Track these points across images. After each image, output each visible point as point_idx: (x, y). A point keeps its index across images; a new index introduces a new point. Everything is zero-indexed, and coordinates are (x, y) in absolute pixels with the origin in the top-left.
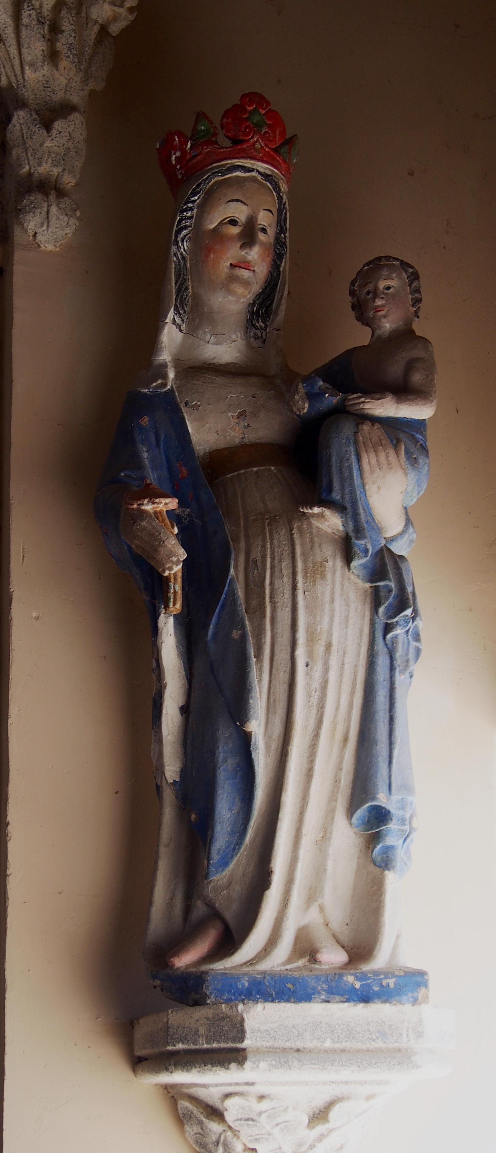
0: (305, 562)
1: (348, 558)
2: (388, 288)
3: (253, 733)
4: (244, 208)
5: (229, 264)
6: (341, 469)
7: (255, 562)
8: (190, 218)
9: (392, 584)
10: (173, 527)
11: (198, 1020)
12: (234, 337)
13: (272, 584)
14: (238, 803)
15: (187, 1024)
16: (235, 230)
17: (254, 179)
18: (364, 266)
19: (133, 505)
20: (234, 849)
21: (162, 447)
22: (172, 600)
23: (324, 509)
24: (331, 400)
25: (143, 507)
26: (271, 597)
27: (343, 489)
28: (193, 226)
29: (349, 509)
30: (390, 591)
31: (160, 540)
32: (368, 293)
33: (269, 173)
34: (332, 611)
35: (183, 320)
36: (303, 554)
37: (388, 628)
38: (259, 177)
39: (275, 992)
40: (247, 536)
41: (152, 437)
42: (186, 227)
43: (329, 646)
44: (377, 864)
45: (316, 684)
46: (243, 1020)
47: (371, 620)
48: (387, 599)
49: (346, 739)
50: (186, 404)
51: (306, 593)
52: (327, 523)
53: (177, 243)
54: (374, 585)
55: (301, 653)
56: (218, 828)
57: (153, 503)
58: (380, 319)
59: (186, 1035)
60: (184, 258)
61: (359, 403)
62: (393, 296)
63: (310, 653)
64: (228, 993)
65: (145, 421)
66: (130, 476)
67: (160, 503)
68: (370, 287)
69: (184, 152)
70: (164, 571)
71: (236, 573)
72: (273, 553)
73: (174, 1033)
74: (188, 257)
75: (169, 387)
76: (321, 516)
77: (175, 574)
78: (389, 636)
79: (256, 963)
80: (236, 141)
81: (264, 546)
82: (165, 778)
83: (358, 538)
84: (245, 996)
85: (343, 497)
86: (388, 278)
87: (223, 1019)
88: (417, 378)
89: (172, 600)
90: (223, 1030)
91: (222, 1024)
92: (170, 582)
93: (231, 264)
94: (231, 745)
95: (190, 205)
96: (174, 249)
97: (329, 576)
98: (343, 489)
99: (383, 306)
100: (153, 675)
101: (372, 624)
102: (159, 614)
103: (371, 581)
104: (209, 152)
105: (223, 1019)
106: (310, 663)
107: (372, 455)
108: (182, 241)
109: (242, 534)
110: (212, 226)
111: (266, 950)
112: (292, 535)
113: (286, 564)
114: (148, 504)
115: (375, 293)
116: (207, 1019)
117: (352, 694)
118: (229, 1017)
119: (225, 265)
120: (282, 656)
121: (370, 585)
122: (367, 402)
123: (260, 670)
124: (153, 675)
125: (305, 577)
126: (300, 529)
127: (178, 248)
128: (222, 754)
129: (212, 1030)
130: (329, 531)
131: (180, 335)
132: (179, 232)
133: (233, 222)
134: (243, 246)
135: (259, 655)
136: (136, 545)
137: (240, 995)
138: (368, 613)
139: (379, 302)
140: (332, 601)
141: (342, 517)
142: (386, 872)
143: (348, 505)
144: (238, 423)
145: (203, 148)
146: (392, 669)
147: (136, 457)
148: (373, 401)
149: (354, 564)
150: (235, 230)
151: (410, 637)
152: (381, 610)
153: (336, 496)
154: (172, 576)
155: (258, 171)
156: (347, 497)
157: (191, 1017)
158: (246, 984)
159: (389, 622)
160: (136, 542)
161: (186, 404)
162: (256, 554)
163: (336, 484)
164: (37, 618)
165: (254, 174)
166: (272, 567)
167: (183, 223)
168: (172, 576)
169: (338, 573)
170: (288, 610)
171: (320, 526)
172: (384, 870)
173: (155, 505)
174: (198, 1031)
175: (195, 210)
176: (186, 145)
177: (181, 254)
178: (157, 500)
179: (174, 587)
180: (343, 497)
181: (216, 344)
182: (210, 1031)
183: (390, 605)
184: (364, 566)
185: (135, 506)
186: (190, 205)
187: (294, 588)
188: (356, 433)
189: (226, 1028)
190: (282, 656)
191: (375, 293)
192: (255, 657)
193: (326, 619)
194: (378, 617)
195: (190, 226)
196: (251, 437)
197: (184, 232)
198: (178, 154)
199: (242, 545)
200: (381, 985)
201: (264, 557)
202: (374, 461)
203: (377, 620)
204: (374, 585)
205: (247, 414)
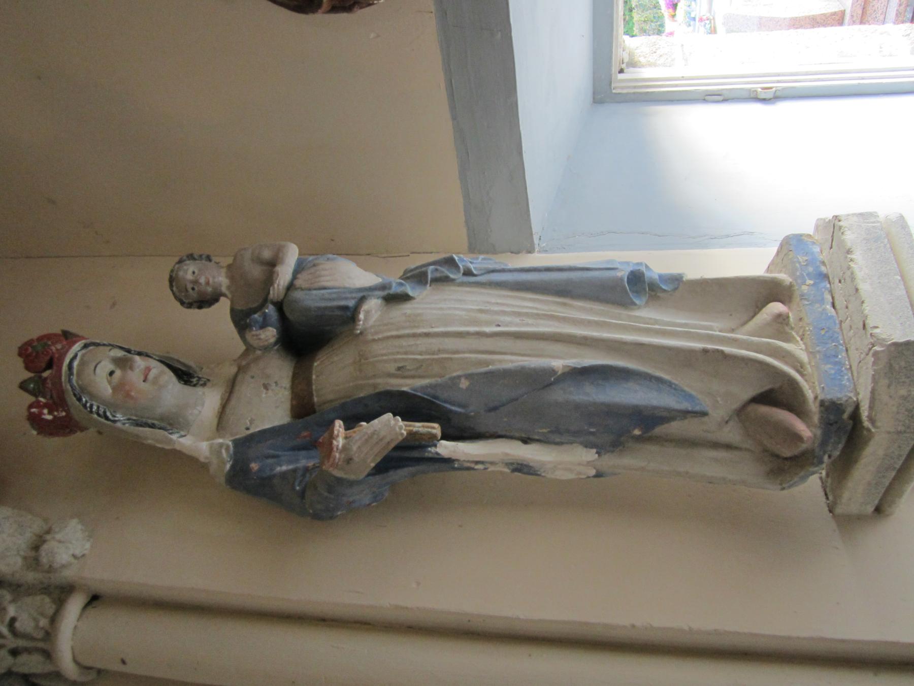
0: (404, 328)
1: (404, 298)
2: (194, 273)
3: (564, 364)
4: (103, 363)
5: (144, 383)
6: (330, 299)
7: (399, 369)
8: (98, 407)
9: (432, 267)
10: (361, 426)
11: (891, 397)
12: (200, 393)
13: (421, 354)
14: (631, 385)
15: (895, 409)
16: (118, 373)
17: (83, 355)
18: (172, 290)
19: (335, 456)
20: (675, 389)
21: (280, 453)
22: (430, 430)
23: (362, 309)
24: (270, 310)
25: (340, 446)
26: (433, 354)
27: (346, 299)
28: (105, 407)
29: (365, 294)
30: (437, 270)
31: (373, 434)
32: (193, 289)
33: (83, 345)
34: (450, 309)
35: (178, 432)
36: (397, 330)
37: (468, 273)
38: (84, 351)
39: (831, 343)
40: (374, 376)
41: (270, 461)
42: (105, 412)
43: (481, 311)
44: (676, 286)
45: (517, 320)
46: (896, 344)
47: (458, 286)
48: (442, 272)
49: (564, 304)
50: (248, 429)
51: (433, 326)
52: (373, 312)
53: (115, 421)
54: (429, 282)
55: (488, 329)
56: (655, 402)
57: (338, 436)
58: (214, 282)
59: (907, 410)
60: (129, 419)
61: (278, 289)
62: (200, 270)
63: (488, 323)
64: (842, 381)
65: (254, 466)
66: (301, 482)
67: (339, 431)
68: (189, 286)
69: (46, 406)
70: (402, 434)
71: (407, 385)
72: (393, 354)
73: (903, 425)
74: (129, 417)
75: (230, 443)
76: (368, 313)
77: (406, 426)
78: (475, 272)
79: (799, 363)
80: (49, 366)
81: (386, 361)
82: (593, 461)
83: (390, 288)
84: (842, 367)
85: (353, 298)
86: (186, 271)
87: (891, 365)
88: (267, 254)
89: (430, 430)
90: (905, 368)
91: (897, 367)
92: (412, 430)
93: (144, 381)
94: (572, 389)
95: (88, 405)
96: (119, 425)
97: (420, 311)
98: (346, 299)
99: (206, 278)
100: (489, 470)
101: (462, 284)
102: (437, 453)
103: (426, 283)
104: (52, 383)
105: (891, 365)
106: (497, 323)
107: (322, 279)
108: (114, 416)
109: (371, 382)
110: (110, 391)
111: (783, 357)
112: (379, 339)
113: (404, 342)
114: (338, 442)
115: (196, 282)
116: (889, 386)
117: (524, 299)
118: (890, 360)
119: (143, 386)
120: (488, 344)
121: (428, 285)
122: (279, 282)
123: (500, 361)
124: (489, 470)
125: (418, 327)
126: (376, 333)
127: (119, 421)
128: (581, 397)
129: (903, 380)
130: (379, 313)
131: (188, 437)
132: (107, 418)
133: (111, 373)
134: (131, 368)
135: (487, 363)
136: (372, 462)
137: (842, 371)
138: (453, 288)
139: (202, 280)
140: (441, 309)
141: (371, 299)
142: (684, 279)
143: (361, 294)
144: (272, 390)
145: (47, 388)
146: (503, 271)
147: (283, 475)
148: (278, 278)
149: (411, 293)
150: (118, 373)
151: (475, 261)
152: (452, 276)
153: (351, 303)
154: (407, 428)
155: (79, 351)
156: (354, 295)
157: (886, 404)
158: (829, 366)
159: (462, 271)
160: (369, 461)
161: (248, 429)
162: (391, 368)
163: (343, 303)
164: (418, 584)
165: (80, 354)
166: (406, 353)
167: (101, 412)
168: (407, 428)
169: (416, 306)
170: (446, 340)
171: (374, 319)
172: (682, 281)
173: (340, 434)
174: (903, 396)
175: (94, 403)
176: (41, 401)
177: (124, 420)
178: (336, 432)
179: (417, 427)
180: (353, 298)
181: (203, 405)
182: (904, 382)
183: (448, 270)
184: (413, 288)
185: (337, 455)
186: (88, 405)
187: (427, 335)
188: (302, 289)
189: (903, 364)
190: (488, 344)
191: (196, 282)
192: (488, 366)
193: (457, 312)
194: (457, 279)
195: (105, 409)
196: (286, 382)
197: (108, 414)
198: (46, 411)
199: (379, 381)
200: (806, 265)
201: (395, 361)
202: (328, 278)
203: (460, 280)
204: (429, 282)
205: (266, 383)
